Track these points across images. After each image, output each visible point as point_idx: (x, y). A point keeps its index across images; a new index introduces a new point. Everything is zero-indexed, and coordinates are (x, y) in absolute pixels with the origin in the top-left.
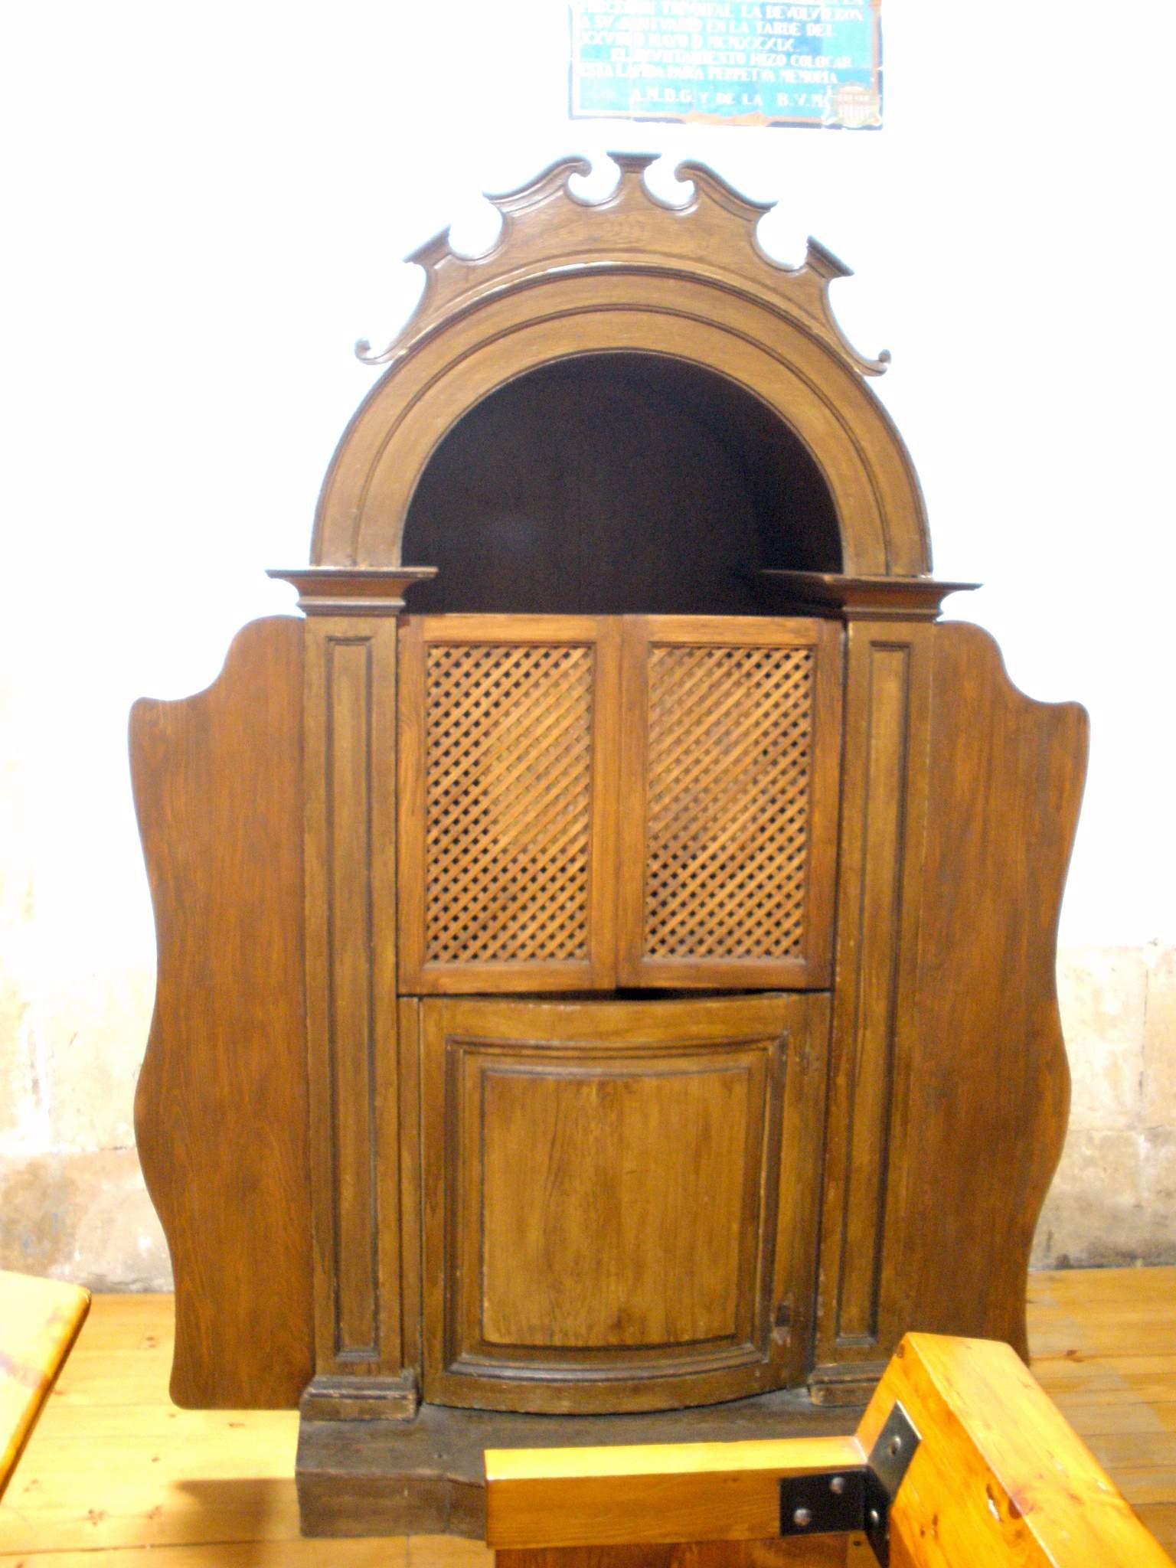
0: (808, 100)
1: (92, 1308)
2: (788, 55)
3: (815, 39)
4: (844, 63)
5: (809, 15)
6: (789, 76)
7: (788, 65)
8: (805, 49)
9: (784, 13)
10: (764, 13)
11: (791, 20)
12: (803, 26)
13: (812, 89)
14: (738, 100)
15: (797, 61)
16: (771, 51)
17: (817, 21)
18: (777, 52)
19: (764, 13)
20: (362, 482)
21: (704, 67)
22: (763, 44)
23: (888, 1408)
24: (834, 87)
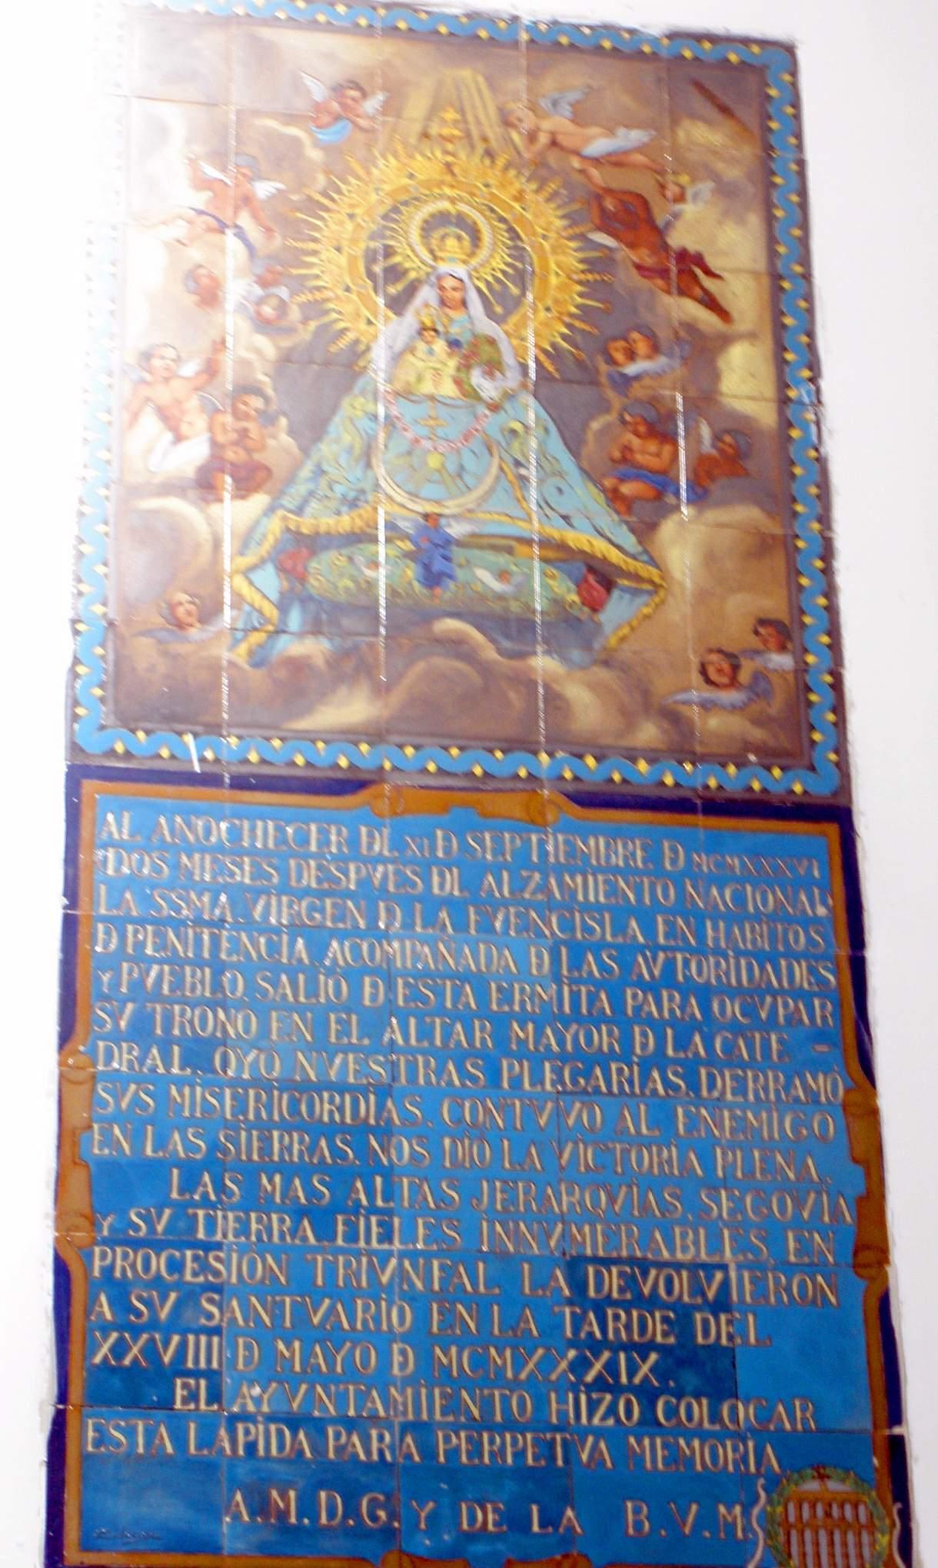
0: (707, 1519)
1: (363, 796)
2: (647, 1395)
3: (715, 1349)
4: (794, 1417)
5: (698, 1290)
6: (652, 1452)
7: (649, 1421)
8: (690, 1379)
9: (630, 1283)
10: (578, 1285)
11: (652, 1302)
12: (681, 1320)
13: (713, 1487)
14: (516, 1522)
15: (672, 1412)
16: (600, 1384)
17: (721, 1305)
18: (616, 1389)
19: (578, 1285)
20: (575, 386)
21: (419, 1428)
22: (581, 1365)
23: (508, 374)
24: (774, 1484)
